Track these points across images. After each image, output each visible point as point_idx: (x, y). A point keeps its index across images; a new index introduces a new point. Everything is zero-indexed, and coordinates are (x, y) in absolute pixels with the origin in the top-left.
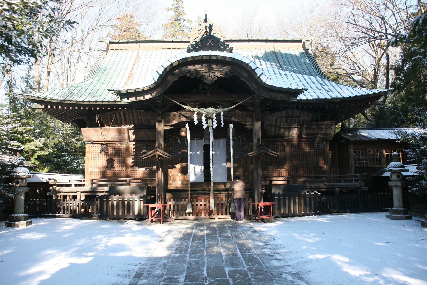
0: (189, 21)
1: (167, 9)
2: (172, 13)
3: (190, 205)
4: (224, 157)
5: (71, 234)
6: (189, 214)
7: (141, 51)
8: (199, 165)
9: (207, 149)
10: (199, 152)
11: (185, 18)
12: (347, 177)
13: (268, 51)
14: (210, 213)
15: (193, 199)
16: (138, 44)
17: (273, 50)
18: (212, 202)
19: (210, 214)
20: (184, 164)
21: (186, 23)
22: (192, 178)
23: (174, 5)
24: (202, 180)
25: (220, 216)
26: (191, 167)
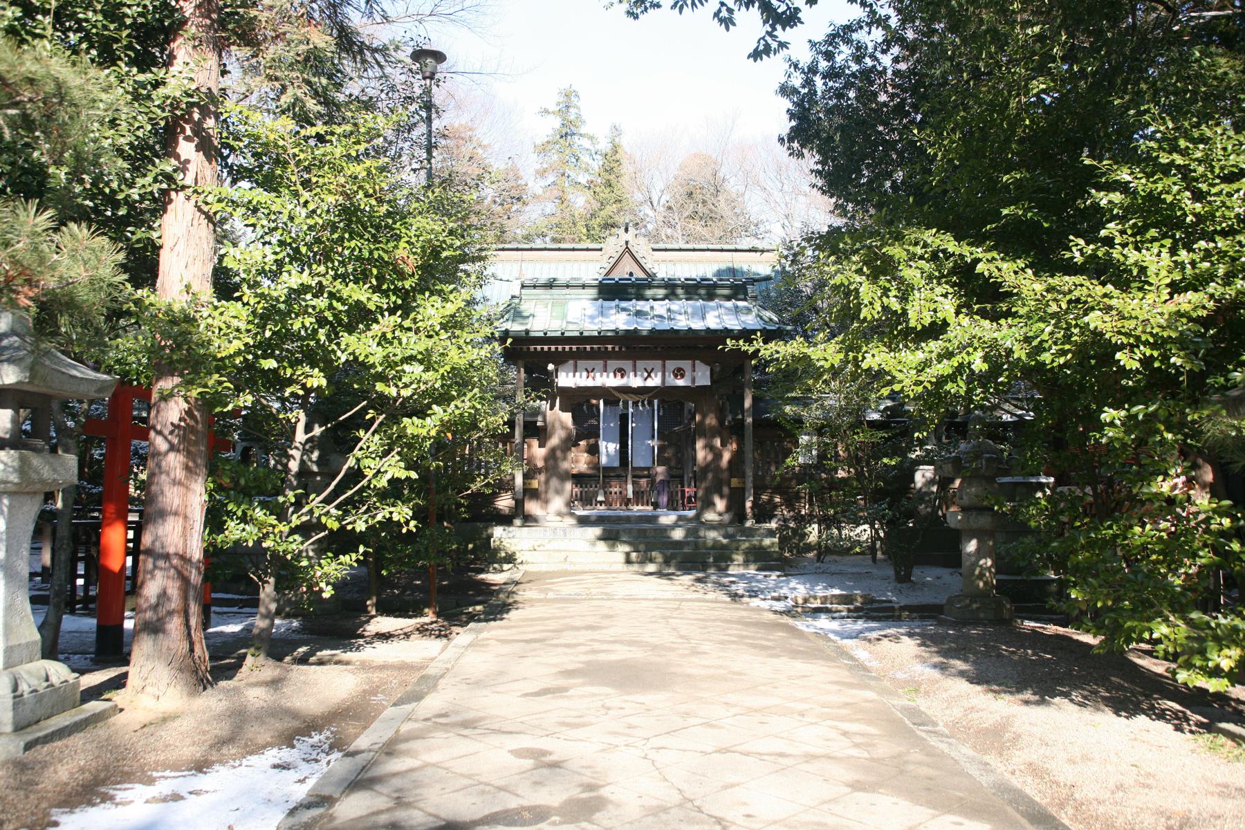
0: (591, 138)
1: (547, 112)
2: (556, 122)
3: (601, 492)
4: (650, 435)
5: (1224, 725)
6: (601, 503)
7: (524, 265)
8: (613, 442)
9: (624, 419)
10: (614, 425)
11: (582, 131)
12: (586, 653)
13: (723, 266)
14: (627, 502)
15: (606, 486)
16: (520, 253)
17: (730, 265)
18: (630, 488)
19: (627, 505)
20: (592, 441)
21: (585, 143)
22: (604, 460)
23: (558, 104)
24: (616, 464)
25: (640, 507)
26: (602, 445)
